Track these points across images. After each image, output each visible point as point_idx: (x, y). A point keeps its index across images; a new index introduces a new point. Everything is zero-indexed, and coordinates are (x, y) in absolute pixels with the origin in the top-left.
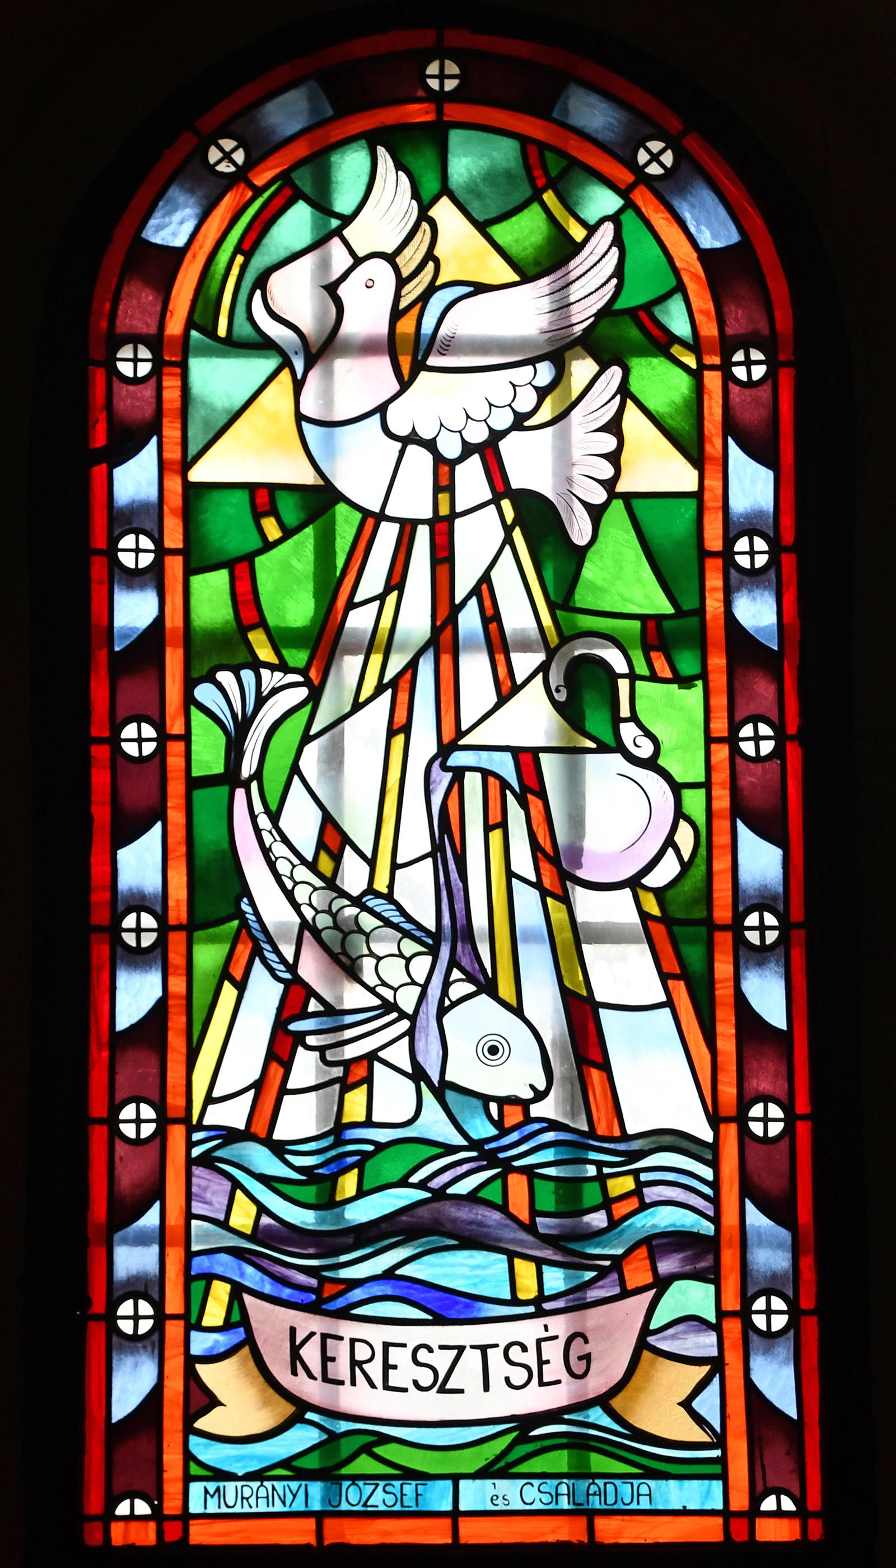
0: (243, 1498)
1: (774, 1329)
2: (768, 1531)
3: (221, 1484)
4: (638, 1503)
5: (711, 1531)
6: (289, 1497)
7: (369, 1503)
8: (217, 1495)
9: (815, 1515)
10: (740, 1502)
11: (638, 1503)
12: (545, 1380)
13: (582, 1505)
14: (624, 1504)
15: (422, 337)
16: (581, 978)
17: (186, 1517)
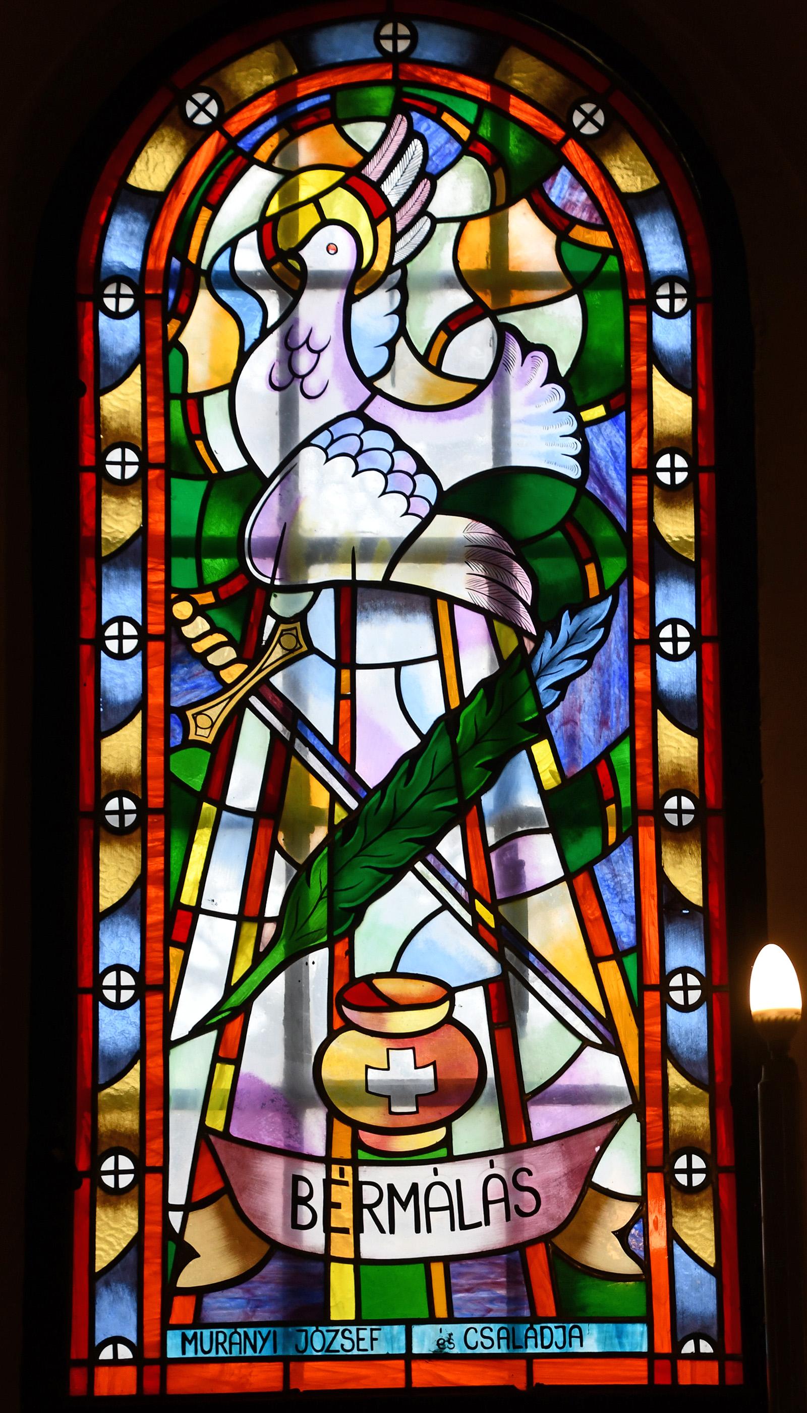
0: (217, 1344)
1: (119, 450)
2: (687, 1375)
3: (199, 1331)
4: (571, 1346)
5: (637, 1373)
6: (260, 1343)
7: (331, 1349)
8: (193, 1343)
9: (732, 1358)
10: (664, 1346)
11: (499, 1347)
12: (467, 1223)
13: (366, 1350)
14: (543, 1347)
15: (623, 811)
16: (520, 829)
17: (164, 1362)
